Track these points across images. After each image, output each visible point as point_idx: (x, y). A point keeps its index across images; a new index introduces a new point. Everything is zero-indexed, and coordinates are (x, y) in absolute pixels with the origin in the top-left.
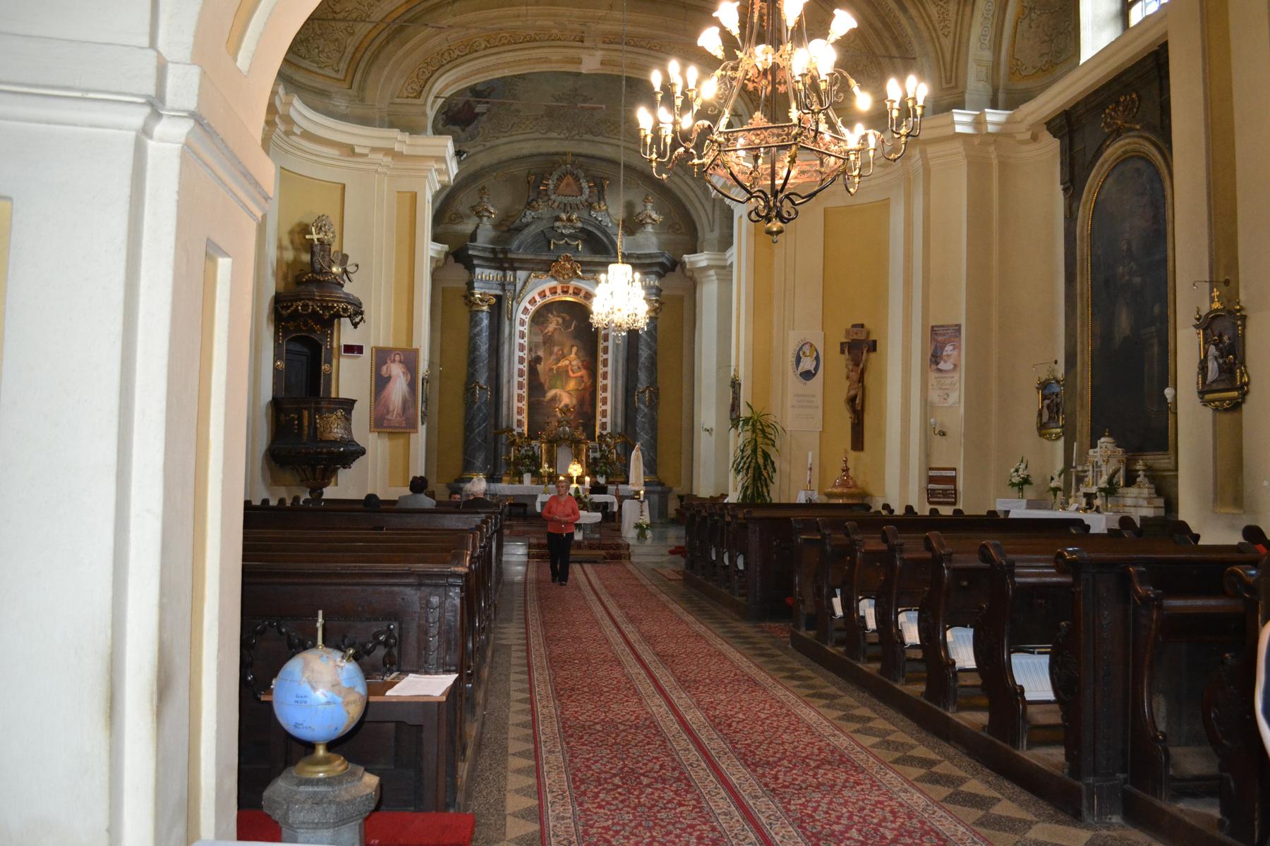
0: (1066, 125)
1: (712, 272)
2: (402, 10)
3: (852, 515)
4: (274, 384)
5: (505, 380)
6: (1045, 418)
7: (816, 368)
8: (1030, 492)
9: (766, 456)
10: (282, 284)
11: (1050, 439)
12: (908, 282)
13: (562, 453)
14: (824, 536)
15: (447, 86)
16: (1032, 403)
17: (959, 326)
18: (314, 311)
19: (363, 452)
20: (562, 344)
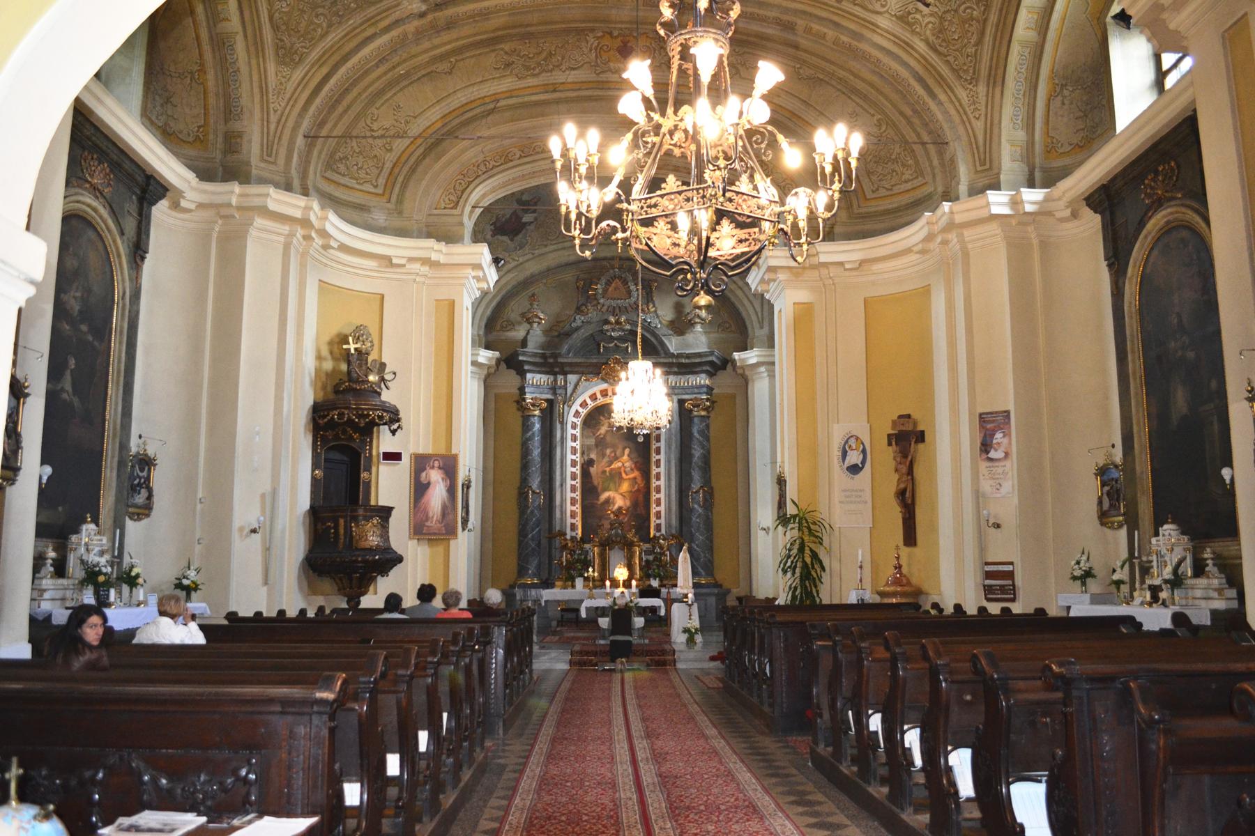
0: (1104, 199)
1: (762, 369)
2: (439, 124)
3: (903, 618)
4: (312, 492)
5: (558, 483)
6: (1106, 505)
7: (863, 462)
8: (1094, 586)
9: (815, 555)
10: (321, 394)
11: (1112, 528)
12: (953, 369)
13: (616, 556)
14: (835, 643)
15: (484, 196)
16: (1089, 492)
17: (1008, 412)
18: (350, 420)
19: (399, 559)
20: (614, 446)
